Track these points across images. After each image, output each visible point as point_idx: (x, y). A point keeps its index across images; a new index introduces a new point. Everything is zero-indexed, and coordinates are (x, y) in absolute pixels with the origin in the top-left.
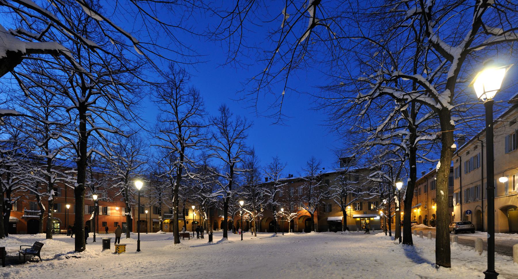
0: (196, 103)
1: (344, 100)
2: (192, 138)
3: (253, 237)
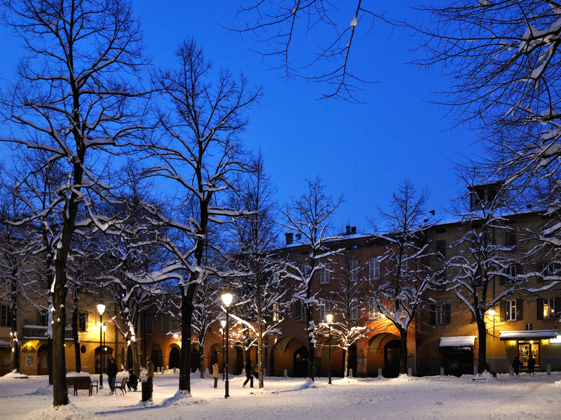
0: (120, 34)
1: (495, 41)
2: (105, 124)
3: (257, 390)
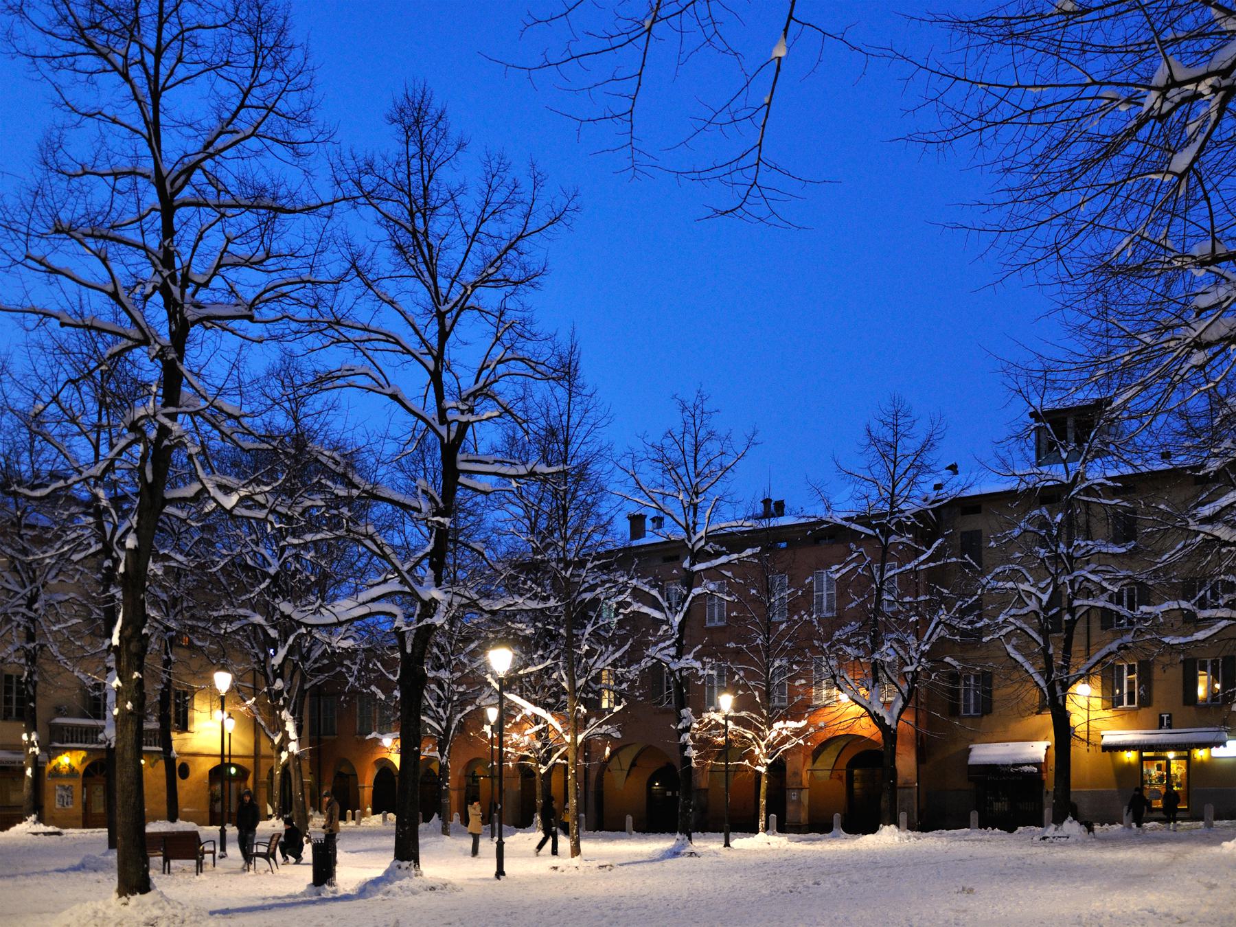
0: (264, 75)
1: (1091, 91)
2: (231, 274)
3: (565, 861)
